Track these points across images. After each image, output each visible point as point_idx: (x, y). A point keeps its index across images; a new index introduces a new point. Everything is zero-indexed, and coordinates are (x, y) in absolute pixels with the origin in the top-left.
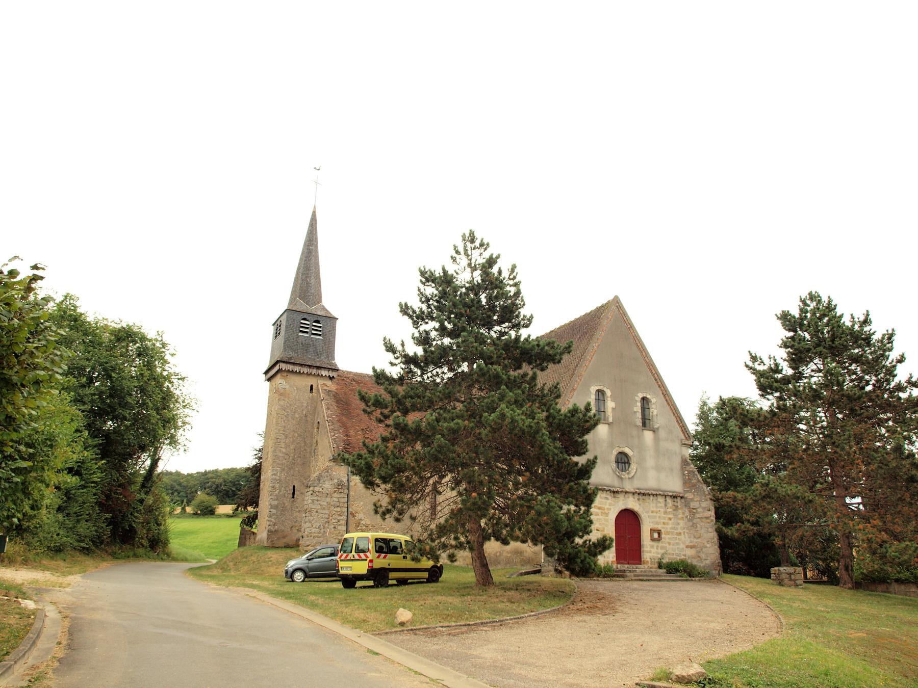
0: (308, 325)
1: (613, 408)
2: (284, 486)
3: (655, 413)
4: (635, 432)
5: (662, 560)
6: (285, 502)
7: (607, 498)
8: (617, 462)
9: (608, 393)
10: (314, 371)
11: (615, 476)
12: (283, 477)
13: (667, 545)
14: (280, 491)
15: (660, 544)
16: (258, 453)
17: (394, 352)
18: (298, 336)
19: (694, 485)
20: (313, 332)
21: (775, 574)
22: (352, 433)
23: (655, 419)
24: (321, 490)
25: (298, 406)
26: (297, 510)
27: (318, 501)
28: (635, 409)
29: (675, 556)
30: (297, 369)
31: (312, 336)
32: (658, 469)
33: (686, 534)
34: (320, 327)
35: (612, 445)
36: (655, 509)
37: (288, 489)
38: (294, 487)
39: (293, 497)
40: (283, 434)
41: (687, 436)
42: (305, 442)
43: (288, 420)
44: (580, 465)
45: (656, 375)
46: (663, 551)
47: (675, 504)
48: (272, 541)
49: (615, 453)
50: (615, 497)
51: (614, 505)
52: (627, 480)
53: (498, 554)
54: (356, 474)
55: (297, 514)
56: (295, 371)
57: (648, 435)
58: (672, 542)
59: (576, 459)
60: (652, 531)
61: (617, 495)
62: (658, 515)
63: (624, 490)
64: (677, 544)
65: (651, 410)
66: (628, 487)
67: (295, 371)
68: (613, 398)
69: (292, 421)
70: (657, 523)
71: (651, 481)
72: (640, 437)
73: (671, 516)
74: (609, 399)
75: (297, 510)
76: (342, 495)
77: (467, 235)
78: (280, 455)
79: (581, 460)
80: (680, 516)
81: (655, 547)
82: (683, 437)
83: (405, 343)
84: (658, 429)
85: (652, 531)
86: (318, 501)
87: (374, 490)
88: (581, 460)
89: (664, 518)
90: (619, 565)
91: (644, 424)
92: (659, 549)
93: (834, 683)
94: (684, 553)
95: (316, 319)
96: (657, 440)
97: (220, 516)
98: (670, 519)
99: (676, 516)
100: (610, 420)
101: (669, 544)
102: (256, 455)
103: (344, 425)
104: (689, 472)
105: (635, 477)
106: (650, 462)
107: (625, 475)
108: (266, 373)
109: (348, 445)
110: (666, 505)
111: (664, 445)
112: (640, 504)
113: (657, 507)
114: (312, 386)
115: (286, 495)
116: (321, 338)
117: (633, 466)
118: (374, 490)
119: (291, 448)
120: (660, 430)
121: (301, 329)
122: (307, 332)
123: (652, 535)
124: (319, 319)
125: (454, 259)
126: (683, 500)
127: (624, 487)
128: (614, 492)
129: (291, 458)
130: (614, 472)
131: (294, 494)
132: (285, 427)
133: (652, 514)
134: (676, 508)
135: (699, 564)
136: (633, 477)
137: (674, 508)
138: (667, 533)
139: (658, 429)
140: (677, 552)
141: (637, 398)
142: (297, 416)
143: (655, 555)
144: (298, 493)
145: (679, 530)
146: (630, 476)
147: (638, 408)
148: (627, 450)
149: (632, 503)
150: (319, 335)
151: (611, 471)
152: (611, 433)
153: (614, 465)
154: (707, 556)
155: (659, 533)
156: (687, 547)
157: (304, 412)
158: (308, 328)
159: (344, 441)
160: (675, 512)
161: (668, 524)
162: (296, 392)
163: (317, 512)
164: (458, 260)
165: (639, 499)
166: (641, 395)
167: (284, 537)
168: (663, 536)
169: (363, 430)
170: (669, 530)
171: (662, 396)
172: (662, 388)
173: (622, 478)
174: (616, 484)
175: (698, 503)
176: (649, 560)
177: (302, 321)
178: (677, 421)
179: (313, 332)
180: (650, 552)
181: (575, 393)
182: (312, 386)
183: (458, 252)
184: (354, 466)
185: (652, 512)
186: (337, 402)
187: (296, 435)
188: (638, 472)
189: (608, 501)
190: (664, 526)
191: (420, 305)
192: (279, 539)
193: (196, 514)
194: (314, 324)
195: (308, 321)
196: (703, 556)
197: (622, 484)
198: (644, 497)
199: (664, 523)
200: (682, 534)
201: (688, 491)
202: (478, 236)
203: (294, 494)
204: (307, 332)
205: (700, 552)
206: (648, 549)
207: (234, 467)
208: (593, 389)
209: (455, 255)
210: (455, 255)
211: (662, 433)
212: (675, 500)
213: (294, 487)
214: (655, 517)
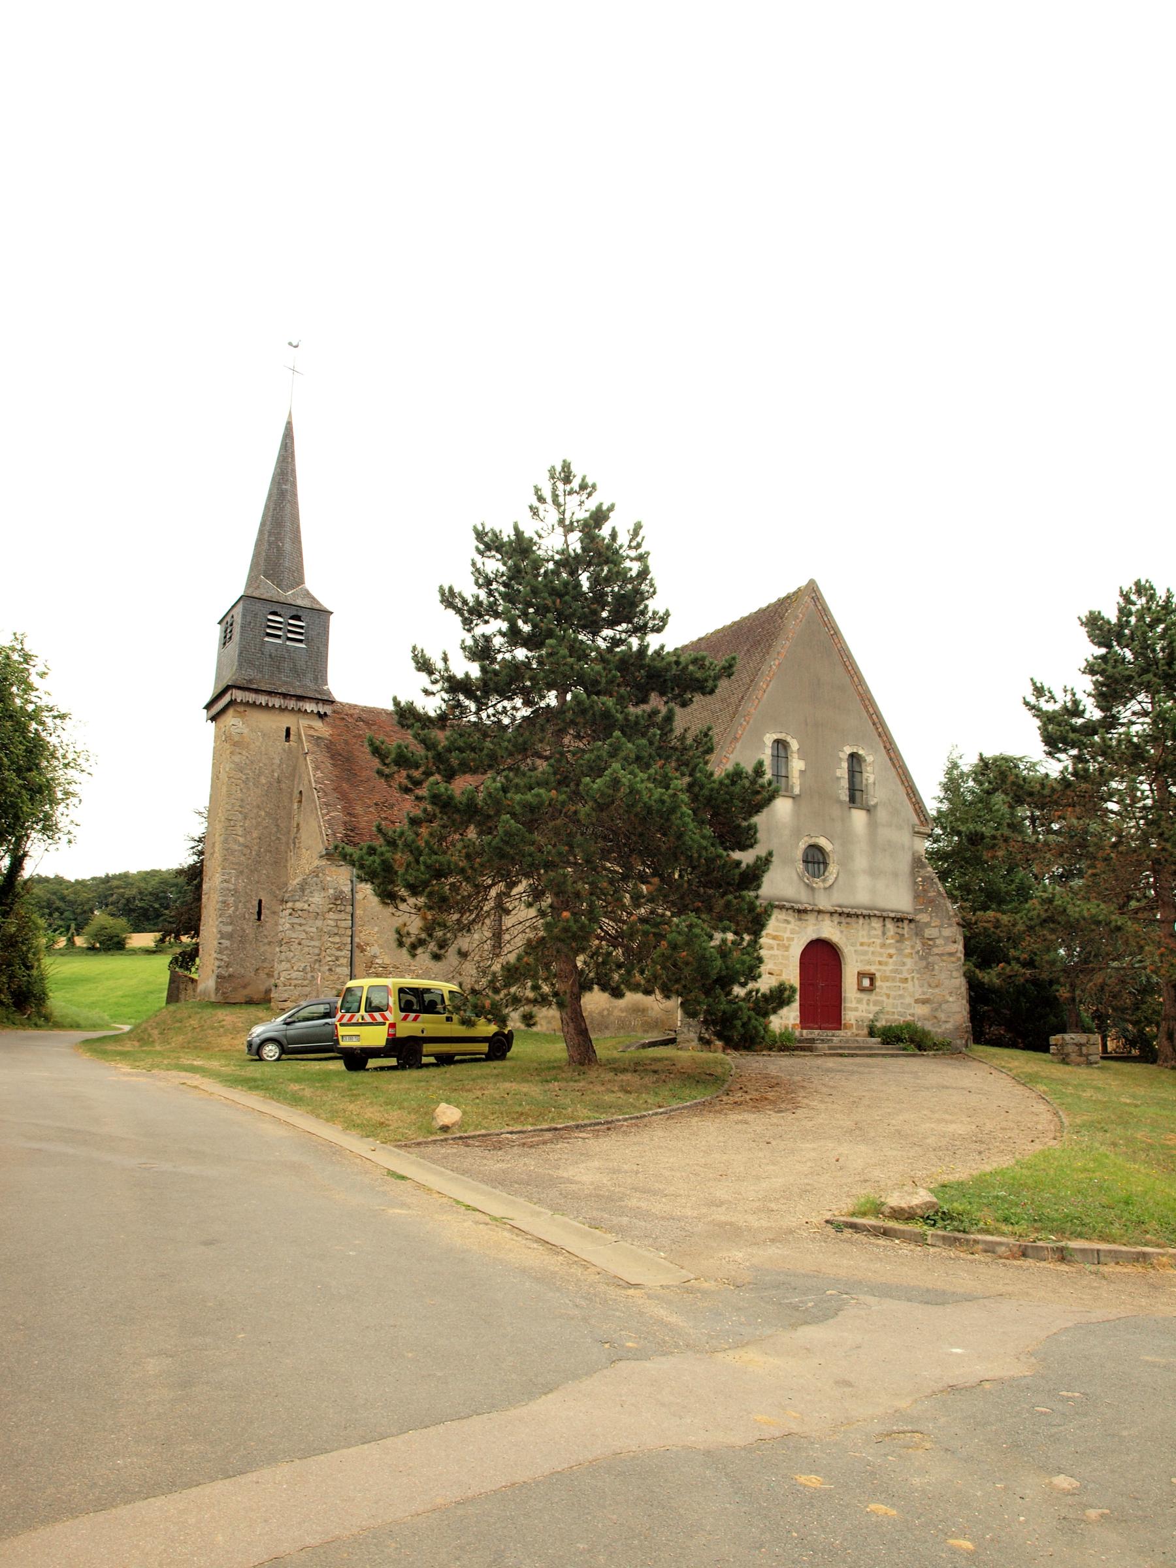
0: (280, 623)
1: (801, 771)
2: (243, 900)
3: (871, 780)
4: (836, 811)
5: (876, 1023)
6: (245, 927)
7: (788, 922)
8: (806, 861)
9: (794, 745)
10: (291, 704)
11: (802, 884)
12: (241, 885)
13: (884, 998)
14: (237, 909)
15: (873, 997)
16: (197, 844)
17: (430, 672)
18: (263, 643)
19: (931, 901)
20: (290, 635)
21: (1056, 1045)
22: (359, 810)
23: (871, 789)
24: (306, 907)
25: (265, 765)
26: (266, 941)
27: (301, 925)
28: (839, 773)
29: (896, 1017)
30: (262, 699)
31: (288, 643)
32: (873, 872)
33: (916, 982)
34: (301, 627)
35: (797, 833)
36: (865, 940)
37: (249, 906)
38: (260, 902)
39: (259, 919)
40: (240, 812)
41: (922, 819)
42: (278, 825)
43: (248, 789)
44: (744, 865)
45: (874, 716)
46: (877, 1008)
47: (900, 931)
48: (224, 993)
49: (802, 845)
50: (800, 919)
51: (798, 933)
52: (822, 891)
53: (605, 1013)
54: (366, 881)
55: (267, 947)
56: (258, 703)
57: (859, 817)
58: (892, 993)
59: (737, 855)
60: (861, 975)
61: (804, 916)
62: (871, 949)
63: (816, 908)
64: (901, 996)
65: (865, 775)
66: (824, 903)
67: (258, 703)
68: (803, 755)
69: (256, 790)
70: (870, 963)
71: (862, 893)
72: (845, 820)
73: (892, 951)
74: (795, 756)
75: (266, 941)
76: (343, 916)
77: (559, 469)
78: (236, 847)
79: (746, 858)
80: (908, 951)
81: (865, 1002)
82: (917, 821)
83: (449, 656)
84: (875, 806)
85: (861, 975)
86: (301, 925)
87: (397, 908)
88: (746, 858)
89: (881, 955)
90: (805, 1032)
91: (852, 799)
92: (871, 1004)
93: (1138, 1217)
94: (911, 1011)
95: (295, 613)
96: (873, 825)
97: (134, 952)
98: (891, 956)
99: (900, 950)
100: (797, 791)
101: (888, 996)
102: (193, 848)
103: (344, 797)
104: (925, 879)
105: (835, 885)
106: (861, 862)
107: (818, 883)
108: (208, 707)
109: (352, 831)
110: (884, 933)
111: (885, 833)
112: (842, 932)
113: (869, 936)
114: (288, 730)
115: (247, 916)
116: (303, 646)
117: (833, 869)
118: (397, 908)
119: (255, 835)
120: (879, 808)
121: (269, 631)
122: (278, 637)
123: (859, 983)
124: (300, 614)
125: (534, 511)
126: (912, 926)
127: (817, 902)
128: (799, 911)
129: (254, 853)
130: (801, 878)
131: (259, 913)
132: (242, 800)
133: (861, 948)
134: (901, 938)
135: (934, 1030)
136: (831, 886)
137: (898, 937)
138: (886, 979)
139: (875, 806)
140: (900, 1009)
141: (841, 755)
142: (264, 781)
143: (864, 1014)
144: (268, 912)
145: (905, 975)
146: (827, 885)
147: (843, 771)
148: (823, 842)
149: (829, 930)
150: (300, 641)
151: (795, 877)
152: (797, 813)
153: (801, 866)
154: (949, 1017)
155: (872, 978)
156: (917, 1001)
157: (276, 775)
158: (280, 629)
159: (345, 823)
160: (898, 944)
161: (886, 964)
162: (261, 739)
163: (300, 944)
164: (541, 513)
165: (840, 923)
166: (848, 750)
167: (245, 987)
168: (878, 983)
169: (376, 804)
170: (888, 974)
171: (883, 751)
172: (885, 738)
173: (813, 889)
174: (802, 896)
175: (937, 929)
176: (853, 1022)
177: (271, 617)
178: (908, 794)
179: (290, 635)
180: (856, 1009)
181: (738, 745)
182: (288, 730)
183: (541, 499)
184: (362, 867)
185: (862, 944)
186: (332, 757)
187: (263, 813)
188: (840, 879)
189: (789, 927)
190: (880, 967)
191: (475, 590)
192: (235, 989)
193: (92, 949)
194: (291, 622)
195: (280, 616)
196: (942, 1016)
197: (814, 898)
198: (849, 920)
199: (880, 963)
200: (909, 980)
201: (921, 911)
202: (578, 471)
203: (259, 913)
204: (278, 637)
205: (936, 1009)
206: (854, 1005)
207: (157, 869)
208: (769, 738)
209: (536, 503)
210: (536, 503)
211: (882, 814)
212: (900, 924)
213: (260, 902)
214: (865, 953)
